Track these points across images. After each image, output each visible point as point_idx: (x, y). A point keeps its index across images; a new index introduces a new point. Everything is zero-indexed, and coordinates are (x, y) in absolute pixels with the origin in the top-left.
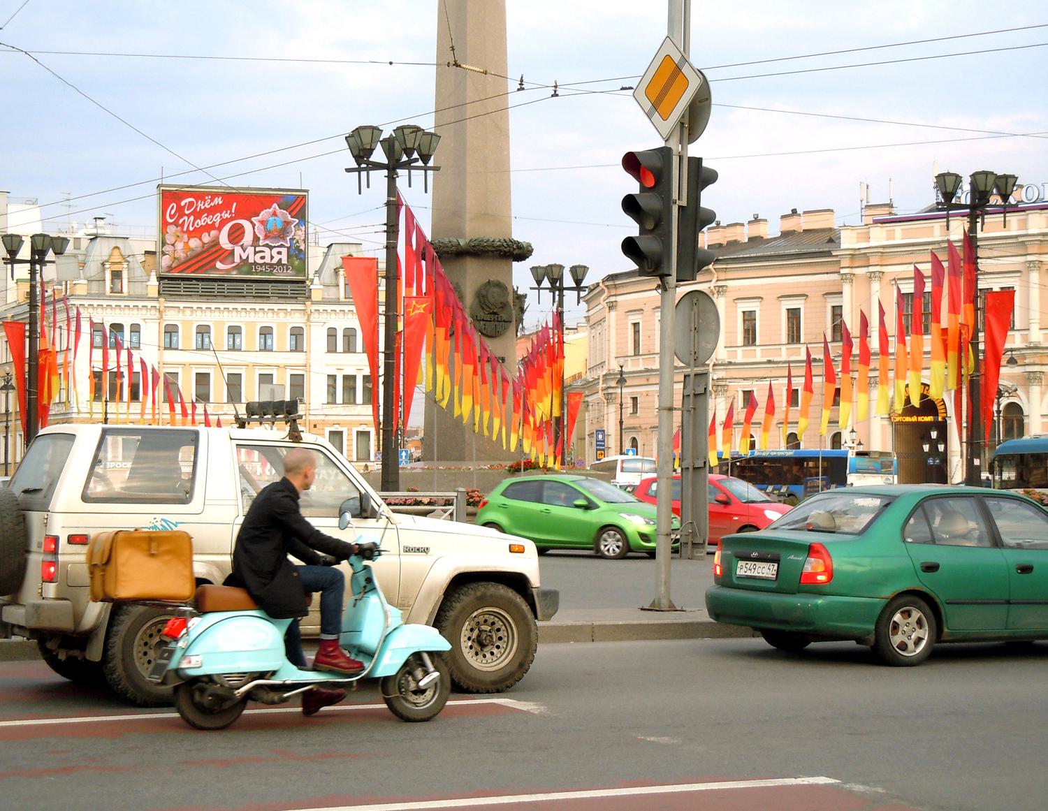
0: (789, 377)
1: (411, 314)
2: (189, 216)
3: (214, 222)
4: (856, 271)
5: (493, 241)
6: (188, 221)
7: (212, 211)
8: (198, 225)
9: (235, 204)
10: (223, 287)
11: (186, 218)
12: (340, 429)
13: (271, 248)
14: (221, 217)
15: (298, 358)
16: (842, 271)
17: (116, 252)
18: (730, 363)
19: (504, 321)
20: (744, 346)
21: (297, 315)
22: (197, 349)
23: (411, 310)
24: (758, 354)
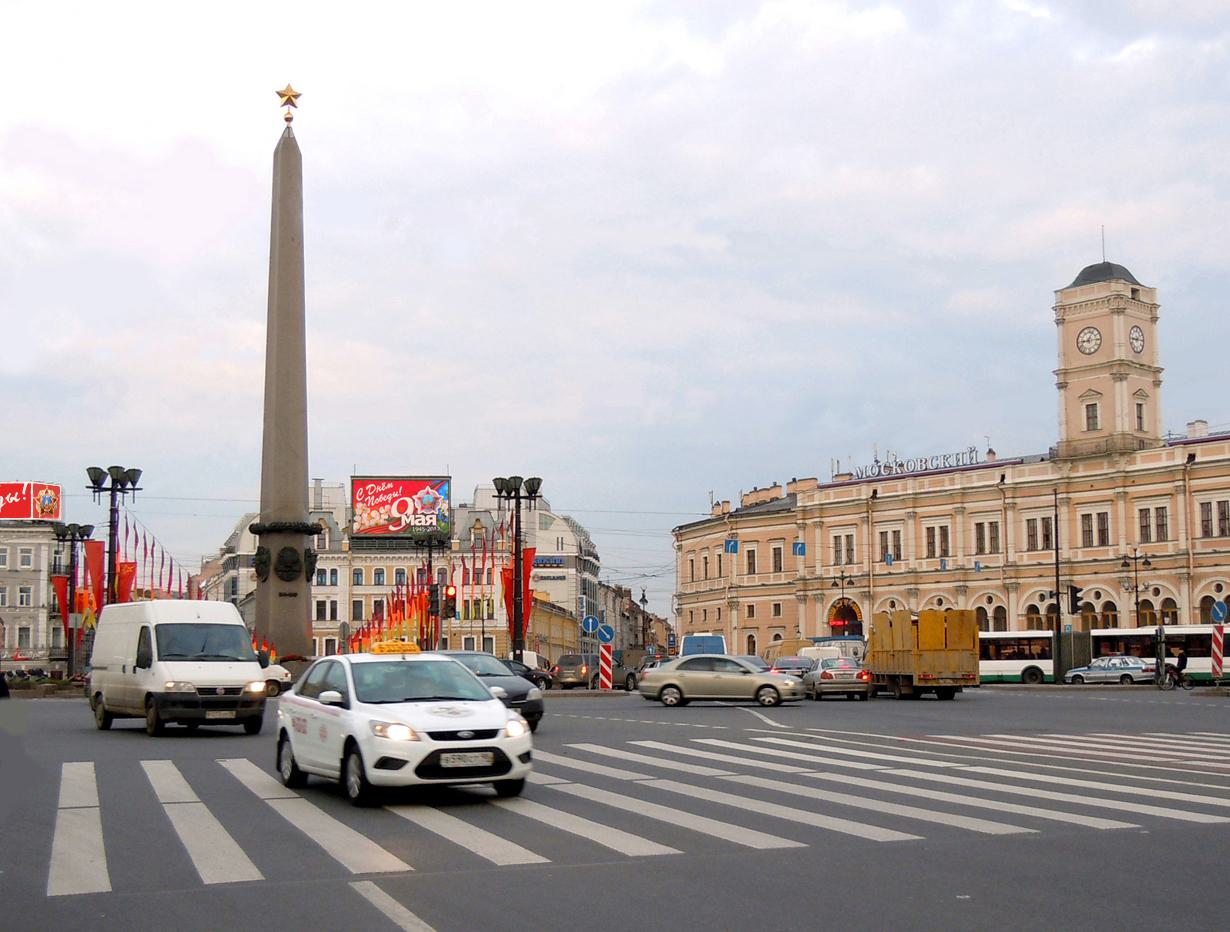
0: (1057, 576)
2: (371, 496)
4: (807, 522)
6: (371, 499)
7: (386, 493)
13: (426, 515)
16: (799, 522)
18: (740, 587)
24: (757, 580)
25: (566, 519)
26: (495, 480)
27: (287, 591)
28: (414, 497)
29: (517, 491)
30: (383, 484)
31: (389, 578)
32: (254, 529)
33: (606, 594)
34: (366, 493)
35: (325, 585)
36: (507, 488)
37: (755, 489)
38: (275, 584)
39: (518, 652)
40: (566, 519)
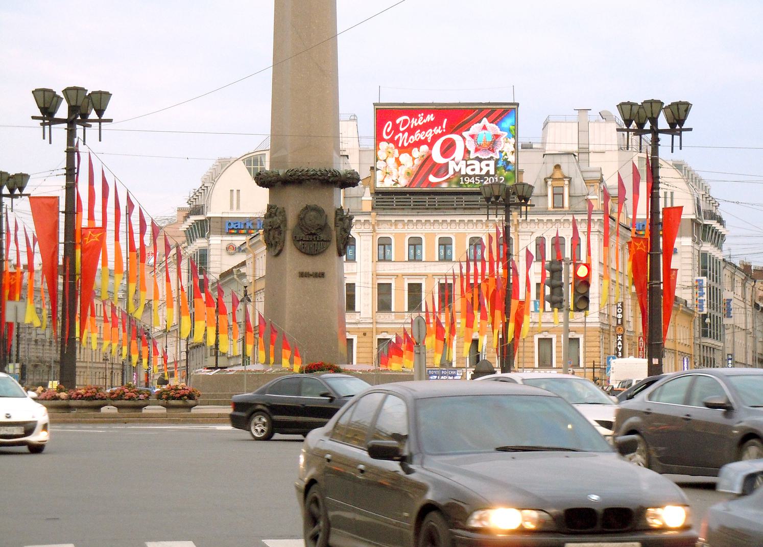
1: (87, 242)
2: (403, 133)
3: (427, 138)
5: (307, 171)
6: (403, 138)
7: (425, 127)
8: (412, 140)
9: (446, 120)
10: (434, 200)
11: (400, 134)
12: (549, 336)
14: (433, 132)
19: (323, 240)
22: (409, 260)
23: (87, 239)
26: (621, 106)
28: (464, 134)
29: (654, 121)
30: (421, 116)
31: (459, 250)
32: (262, 180)
33: (733, 274)
34: (396, 129)
36: (639, 118)
38: (292, 258)
39: (655, 361)
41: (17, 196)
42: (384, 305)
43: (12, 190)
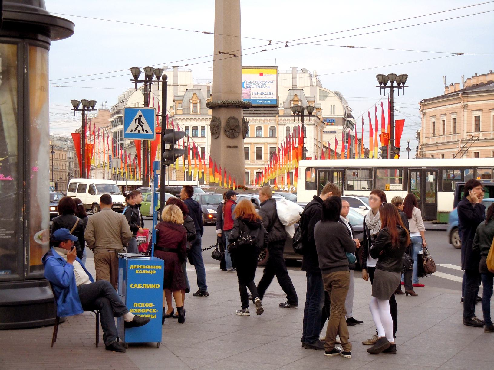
15: (272, 140)
17: (195, 95)
20: (475, 132)
21: (273, 121)
25: (337, 94)
27: (232, 145)
29: (392, 83)
35: (197, 137)
37: (476, 74)
38: (223, 139)
40: (337, 94)
41: (90, 110)
42: (259, 157)
43: (399, 84)
